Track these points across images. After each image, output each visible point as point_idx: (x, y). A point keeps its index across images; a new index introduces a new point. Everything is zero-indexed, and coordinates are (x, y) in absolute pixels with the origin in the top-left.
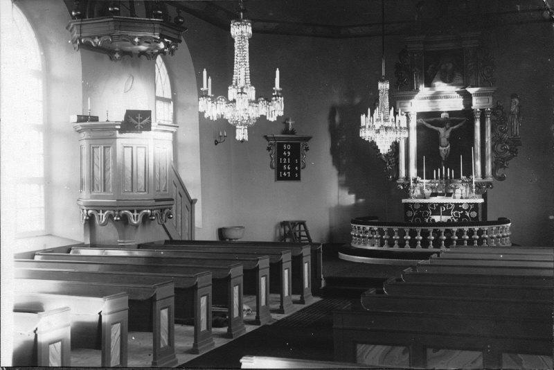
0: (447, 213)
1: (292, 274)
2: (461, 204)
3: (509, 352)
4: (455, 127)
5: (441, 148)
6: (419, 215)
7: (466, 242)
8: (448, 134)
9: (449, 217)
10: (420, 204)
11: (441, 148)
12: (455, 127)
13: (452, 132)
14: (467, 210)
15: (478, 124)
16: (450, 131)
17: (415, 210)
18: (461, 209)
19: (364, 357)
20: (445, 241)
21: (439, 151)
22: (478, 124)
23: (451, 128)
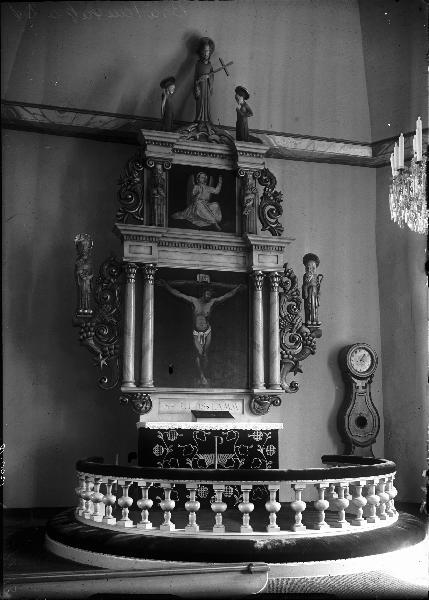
0: (226, 448)
1: (222, 387)
2: (251, 432)
3: (99, 468)
4: (220, 299)
5: (195, 333)
6: (177, 453)
7: (275, 516)
8: (207, 308)
9: (231, 456)
10: (179, 430)
11: (195, 333)
12: (220, 299)
13: (215, 307)
14: (261, 443)
15: (260, 294)
16: (211, 303)
17: (169, 443)
18: (253, 440)
19: (84, 507)
20: (224, 514)
21: (192, 337)
22: (260, 294)
23: (213, 300)
